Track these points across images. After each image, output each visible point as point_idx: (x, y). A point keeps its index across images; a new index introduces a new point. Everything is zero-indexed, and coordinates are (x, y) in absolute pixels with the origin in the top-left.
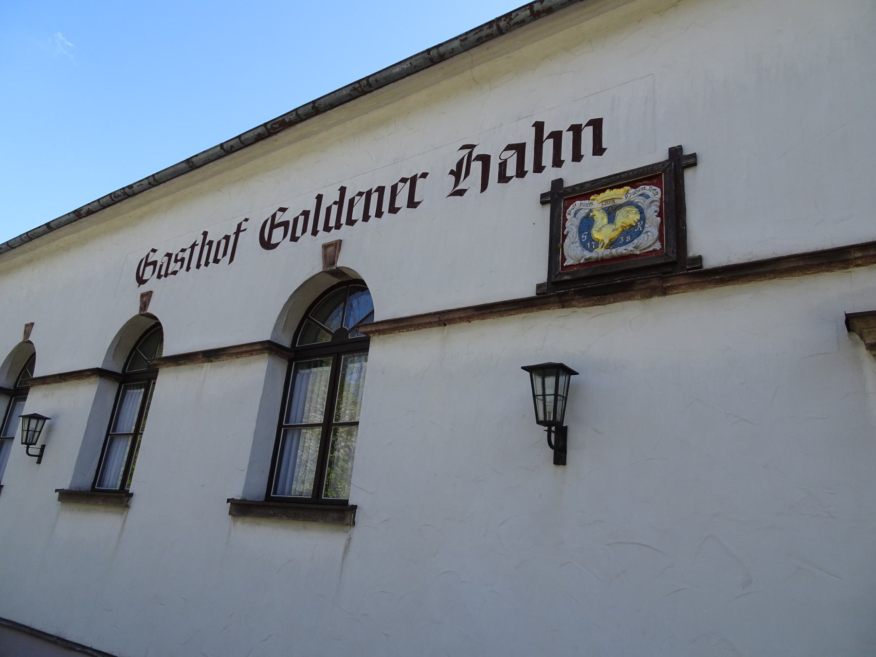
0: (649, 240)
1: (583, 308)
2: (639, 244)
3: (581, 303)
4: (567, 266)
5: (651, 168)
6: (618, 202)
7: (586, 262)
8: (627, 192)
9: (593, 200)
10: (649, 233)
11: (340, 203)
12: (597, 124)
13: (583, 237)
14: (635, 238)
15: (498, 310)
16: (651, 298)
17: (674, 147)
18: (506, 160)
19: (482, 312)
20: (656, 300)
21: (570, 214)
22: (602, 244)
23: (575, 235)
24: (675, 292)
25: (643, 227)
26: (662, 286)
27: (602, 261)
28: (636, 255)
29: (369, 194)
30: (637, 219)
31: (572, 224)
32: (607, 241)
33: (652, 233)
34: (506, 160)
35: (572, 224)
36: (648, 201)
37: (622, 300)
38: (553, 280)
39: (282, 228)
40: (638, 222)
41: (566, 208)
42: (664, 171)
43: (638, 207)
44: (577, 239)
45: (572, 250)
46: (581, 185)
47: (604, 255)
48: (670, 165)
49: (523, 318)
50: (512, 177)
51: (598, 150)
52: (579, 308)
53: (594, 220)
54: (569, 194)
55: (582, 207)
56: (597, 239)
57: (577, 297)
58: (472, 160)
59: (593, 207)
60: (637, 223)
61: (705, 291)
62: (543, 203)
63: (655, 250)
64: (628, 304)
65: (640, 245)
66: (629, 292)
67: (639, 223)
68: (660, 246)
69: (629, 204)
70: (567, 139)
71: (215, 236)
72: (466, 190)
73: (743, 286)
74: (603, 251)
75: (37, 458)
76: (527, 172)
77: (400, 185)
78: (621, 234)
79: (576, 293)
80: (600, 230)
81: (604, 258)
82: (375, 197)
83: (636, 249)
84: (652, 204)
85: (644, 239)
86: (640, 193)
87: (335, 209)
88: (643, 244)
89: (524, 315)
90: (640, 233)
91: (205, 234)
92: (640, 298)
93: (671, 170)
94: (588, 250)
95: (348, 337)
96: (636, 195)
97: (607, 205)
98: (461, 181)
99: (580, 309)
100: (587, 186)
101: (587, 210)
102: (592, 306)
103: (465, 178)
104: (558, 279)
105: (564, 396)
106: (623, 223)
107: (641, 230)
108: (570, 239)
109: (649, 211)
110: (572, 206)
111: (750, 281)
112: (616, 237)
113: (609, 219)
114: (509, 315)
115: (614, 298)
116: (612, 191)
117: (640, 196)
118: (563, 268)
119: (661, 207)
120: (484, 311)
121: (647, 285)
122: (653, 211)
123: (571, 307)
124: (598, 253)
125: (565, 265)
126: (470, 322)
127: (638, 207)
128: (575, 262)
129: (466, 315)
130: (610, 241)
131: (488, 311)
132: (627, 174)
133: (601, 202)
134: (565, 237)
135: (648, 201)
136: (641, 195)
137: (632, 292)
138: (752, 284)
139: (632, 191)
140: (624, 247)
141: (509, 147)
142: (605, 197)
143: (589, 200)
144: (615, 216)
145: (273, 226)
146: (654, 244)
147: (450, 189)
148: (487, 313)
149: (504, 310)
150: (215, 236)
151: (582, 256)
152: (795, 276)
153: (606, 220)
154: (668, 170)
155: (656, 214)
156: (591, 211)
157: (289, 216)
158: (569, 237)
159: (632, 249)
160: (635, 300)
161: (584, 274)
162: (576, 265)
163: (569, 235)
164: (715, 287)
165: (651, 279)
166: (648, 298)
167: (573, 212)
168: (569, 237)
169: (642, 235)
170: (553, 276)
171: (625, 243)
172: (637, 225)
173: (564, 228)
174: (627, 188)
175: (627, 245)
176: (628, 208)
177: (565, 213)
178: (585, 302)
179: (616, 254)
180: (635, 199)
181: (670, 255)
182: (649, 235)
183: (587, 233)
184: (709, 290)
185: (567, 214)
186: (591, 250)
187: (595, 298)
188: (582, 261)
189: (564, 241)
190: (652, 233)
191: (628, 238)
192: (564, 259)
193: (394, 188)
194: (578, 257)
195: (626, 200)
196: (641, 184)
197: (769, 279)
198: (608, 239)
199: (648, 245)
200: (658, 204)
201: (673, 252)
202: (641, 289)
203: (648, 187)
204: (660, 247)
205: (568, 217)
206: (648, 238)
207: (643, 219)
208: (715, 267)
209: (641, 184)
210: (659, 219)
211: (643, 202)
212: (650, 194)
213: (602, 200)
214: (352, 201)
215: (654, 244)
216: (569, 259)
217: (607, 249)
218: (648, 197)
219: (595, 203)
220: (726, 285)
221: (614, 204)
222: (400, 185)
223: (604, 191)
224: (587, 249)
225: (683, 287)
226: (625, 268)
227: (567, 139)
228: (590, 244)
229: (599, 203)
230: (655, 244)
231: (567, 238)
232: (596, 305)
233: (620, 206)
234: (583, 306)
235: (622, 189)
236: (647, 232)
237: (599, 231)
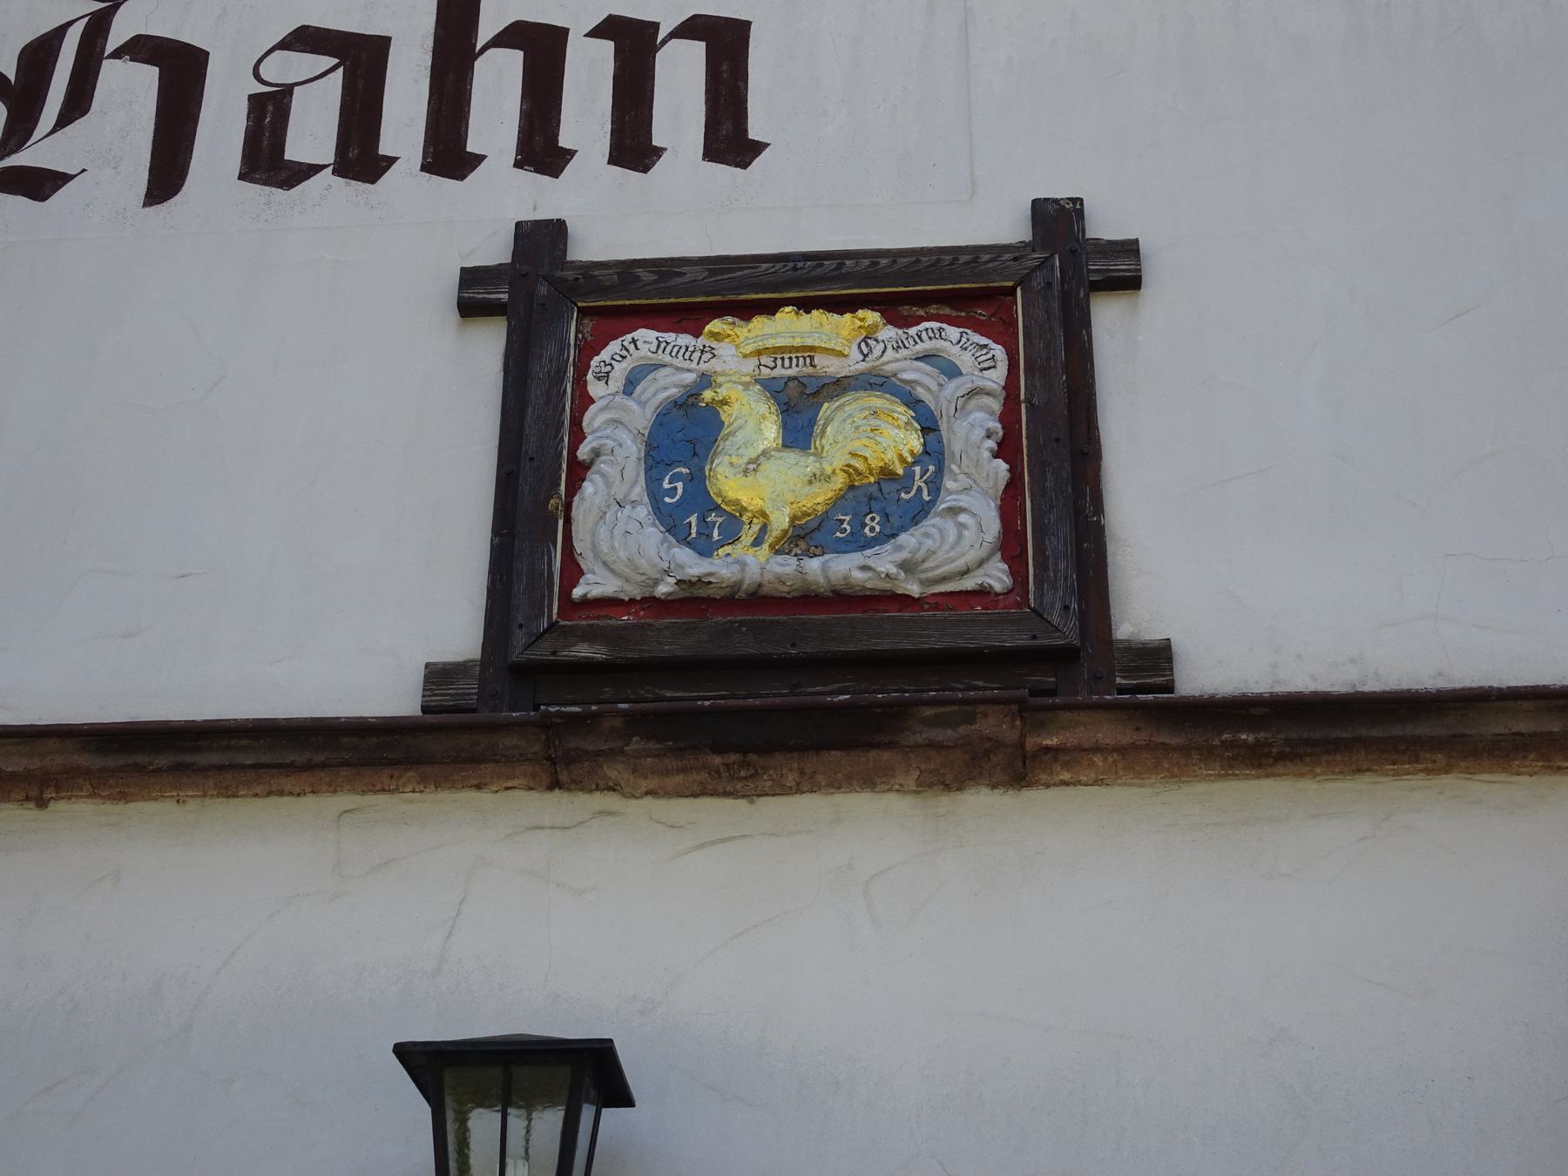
0: (966, 542)
1: (648, 800)
2: (921, 554)
3: (646, 778)
4: (588, 603)
5: (966, 258)
6: (830, 367)
7: (682, 595)
8: (869, 337)
9: (716, 336)
10: (963, 518)
13: (666, 485)
14: (903, 528)
15: (214, 758)
16: (960, 789)
17: (1056, 201)
18: (286, 91)
19: (122, 760)
20: (980, 802)
21: (605, 377)
22: (756, 528)
23: (630, 474)
24: (1066, 776)
25: (935, 486)
26: (1022, 746)
27: (756, 600)
28: (905, 600)
30: (912, 453)
31: (616, 422)
32: (780, 521)
33: (974, 515)
34: (286, 91)
35: (616, 422)
36: (954, 388)
37: (838, 784)
38: (518, 649)
40: (914, 463)
41: (589, 349)
42: (1023, 281)
43: (913, 403)
44: (639, 492)
45: (618, 532)
46: (667, 269)
47: (768, 577)
48: (1044, 263)
49: (601, 813)
50: (315, 169)
52: (634, 797)
53: (723, 423)
54: (604, 291)
55: (667, 359)
56: (737, 502)
57: (636, 744)
58: (110, 48)
59: (715, 365)
60: (909, 467)
61: (1185, 789)
62: (471, 305)
63: (983, 593)
64: (859, 804)
65: (923, 561)
66: (873, 754)
67: (917, 469)
68: (1005, 578)
69: (876, 382)
72: (64, 178)
73: (1330, 785)
74: (762, 559)
76: (391, 161)
78: (838, 501)
79: (638, 723)
80: (752, 466)
81: (765, 590)
83: (905, 572)
84: (973, 403)
85: (943, 538)
86: (920, 347)
88: (941, 556)
89: (345, 800)
90: (919, 512)
92: (912, 785)
93: (1049, 284)
94: (689, 544)
96: (904, 352)
97: (779, 372)
98: (37, 134)
99: (634, 802)
100: (692, 273)
101: (690, 377)
102: (695, 795)
103: (64, 120)
104: (542, 653)
106: (853, 455)
107: (926, 498)
108: (609, 485)
109: (961, 427)
110: (614, 347)
111: (1359, 771)
112: (820, 508)
113: (785, 427)
114: (269, 794)
115: (802, 773)
116: (805, 317)
117: (916, 359)
118: (571, 606)
119: (1008, 417)
120: (141, 759)
121: (963, 730)
122: (979, 433)
123: (590, 791)
124: (743, 564)
125: (577, 592)
126: (42, 804)
127: (913, 403)
128: (628, 588)
129: (35, 764)
130: (793, 519)
131: (163, 760)
132: (866, 262)
133: (751, 354)
134: (579, 471)
135: (954, 388)
136: (925, 357)
137: (886, 756)
138: (1362, 785)
139: (889, 333)
140: (857, 558)
141: (305, 39)
142: (772, 336)
143: (697, 335)
144: (812, 422)
146: (981, 563)
148: (159, 770)
149: (257, 766)
151: (665, 565)
152: (1519, 774)
153: (771, 432)
154: (1038, 281)
155: (991, 444)
156: (706, 380)
158: (603, 476)
159: (893, 570)
160: (890, 790)
161: (671, 648)
162: (632, 601)
163: (602, 465)
164: (1220, 777)
165: (981, 708)
166: (947, 787)
167: (620, 371)
168: (603, 476)
169: (931, 523)
170: (520, 639)
171: (859, 543)
172: (909, 475)
173: (578, 436)
174: (872, 317)
175: (868, 552)
176: (877, 401)
177: (582, 369)
178: (666, 773)
179: (822, 580)
180: (904, 370)
181: (1055, 619)
182: (962, 526)
183: (685, 470)
184: (1200, 787)
185: (590, 376)
186: (705, 548)
187: (717, 760)
188: (663, 589)
189: (574, 486)
190: (974, 515)
191: (873, 525)
192: (573, 571)
194: (643, 564)
195: (862, 366)
196: (921, 312)
197: (1427, 771)
198: (788, 510)
199: (960, 564)
200: (996, 406)
201: (1066, 608)
202: (931, 745)
203: (953, 332)
204: (1008, 581)
205: (595, 388)
206: (960, 536)
207: (934, 453)
208: (1244, 695)
209: (921, 312)
210: (1001, 466)
211: (934, 387)
212: (965, 360)
213: (761, 345)
215: (981, 563)
216: (599, 569)
217: (777, 552)
218: (952, 371)
219: (724, 349)
220: (1268, 776)
221: (810, 370)
223: (770, 308)
224: (685, 541)
225: (1098, 759)
226: (861, 647)
228: (702, 520)
229: (745, 356)
230: (985, 566)
231: (590, 475)
232: (714, 794)
233: (839, 386)
234: (650, 793)
235: (848, 316)
236: (954, 511)
237: (746, 472)
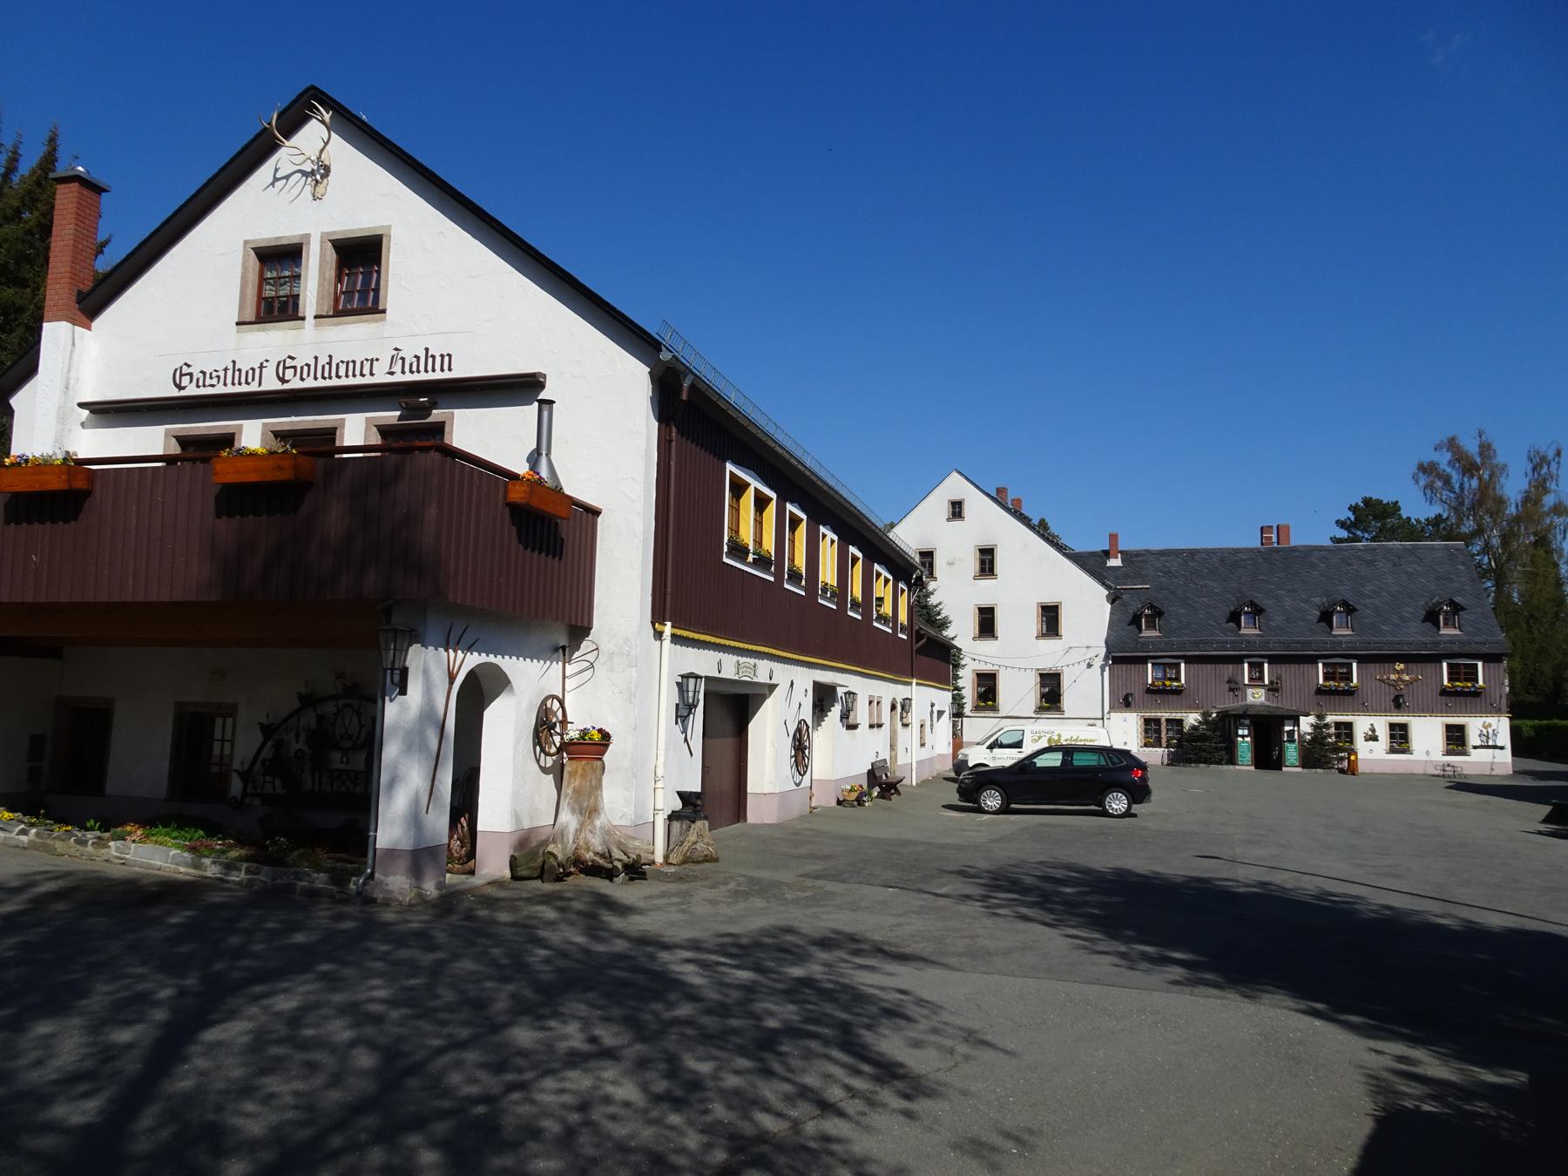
11: (330, 364)
12: (450, 356)
29: (348, 363)
39: (188, 377)
51: (450, 369)
70: (438, 360)
71: (244, 366)
75: (272, 792)
77: (341, 364)
82: (351, 365)
87: (327, 367)
91: (427, 350)
95: (736, 463)
105: (734, 528)
145: (182, 375)
147: (387, 370)
150: (244, 366)
157: (298, 363)
193: (261, 367)
214: (338, 365)
222: (341, 364)
227: (438, 360)
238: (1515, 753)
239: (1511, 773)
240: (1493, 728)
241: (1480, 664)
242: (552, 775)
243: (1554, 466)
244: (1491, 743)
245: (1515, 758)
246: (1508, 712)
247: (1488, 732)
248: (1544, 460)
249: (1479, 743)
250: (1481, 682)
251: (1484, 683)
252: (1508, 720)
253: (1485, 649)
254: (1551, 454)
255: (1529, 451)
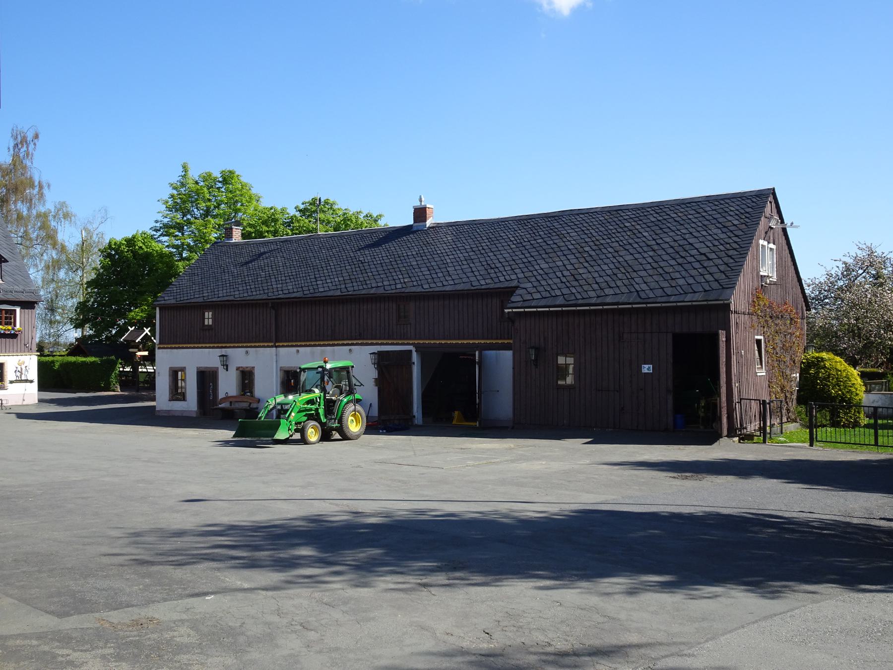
238: (42, 387)
239: (37, 402)
240: (25, 365)
241: (18, 310)
242: (300, 438)
243: (31, 146)
244: (23, 378)
245: (40, 392)
246: (37, 351)
247: (21, 369)
248: (24, 141)
249: (14, 378)
250: (18, 326)
251: (21, 327)
252: (36, 357)
253: (23, 297)
254: (30, 137)
255: (13, 130)
